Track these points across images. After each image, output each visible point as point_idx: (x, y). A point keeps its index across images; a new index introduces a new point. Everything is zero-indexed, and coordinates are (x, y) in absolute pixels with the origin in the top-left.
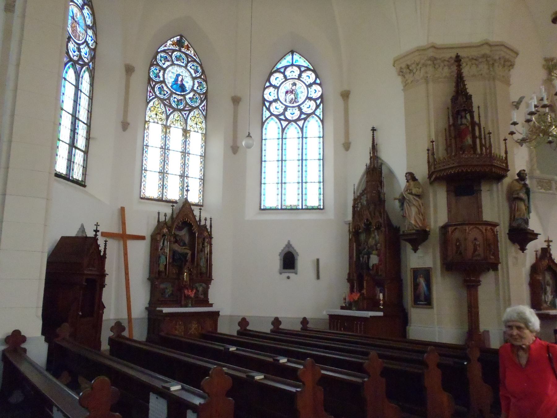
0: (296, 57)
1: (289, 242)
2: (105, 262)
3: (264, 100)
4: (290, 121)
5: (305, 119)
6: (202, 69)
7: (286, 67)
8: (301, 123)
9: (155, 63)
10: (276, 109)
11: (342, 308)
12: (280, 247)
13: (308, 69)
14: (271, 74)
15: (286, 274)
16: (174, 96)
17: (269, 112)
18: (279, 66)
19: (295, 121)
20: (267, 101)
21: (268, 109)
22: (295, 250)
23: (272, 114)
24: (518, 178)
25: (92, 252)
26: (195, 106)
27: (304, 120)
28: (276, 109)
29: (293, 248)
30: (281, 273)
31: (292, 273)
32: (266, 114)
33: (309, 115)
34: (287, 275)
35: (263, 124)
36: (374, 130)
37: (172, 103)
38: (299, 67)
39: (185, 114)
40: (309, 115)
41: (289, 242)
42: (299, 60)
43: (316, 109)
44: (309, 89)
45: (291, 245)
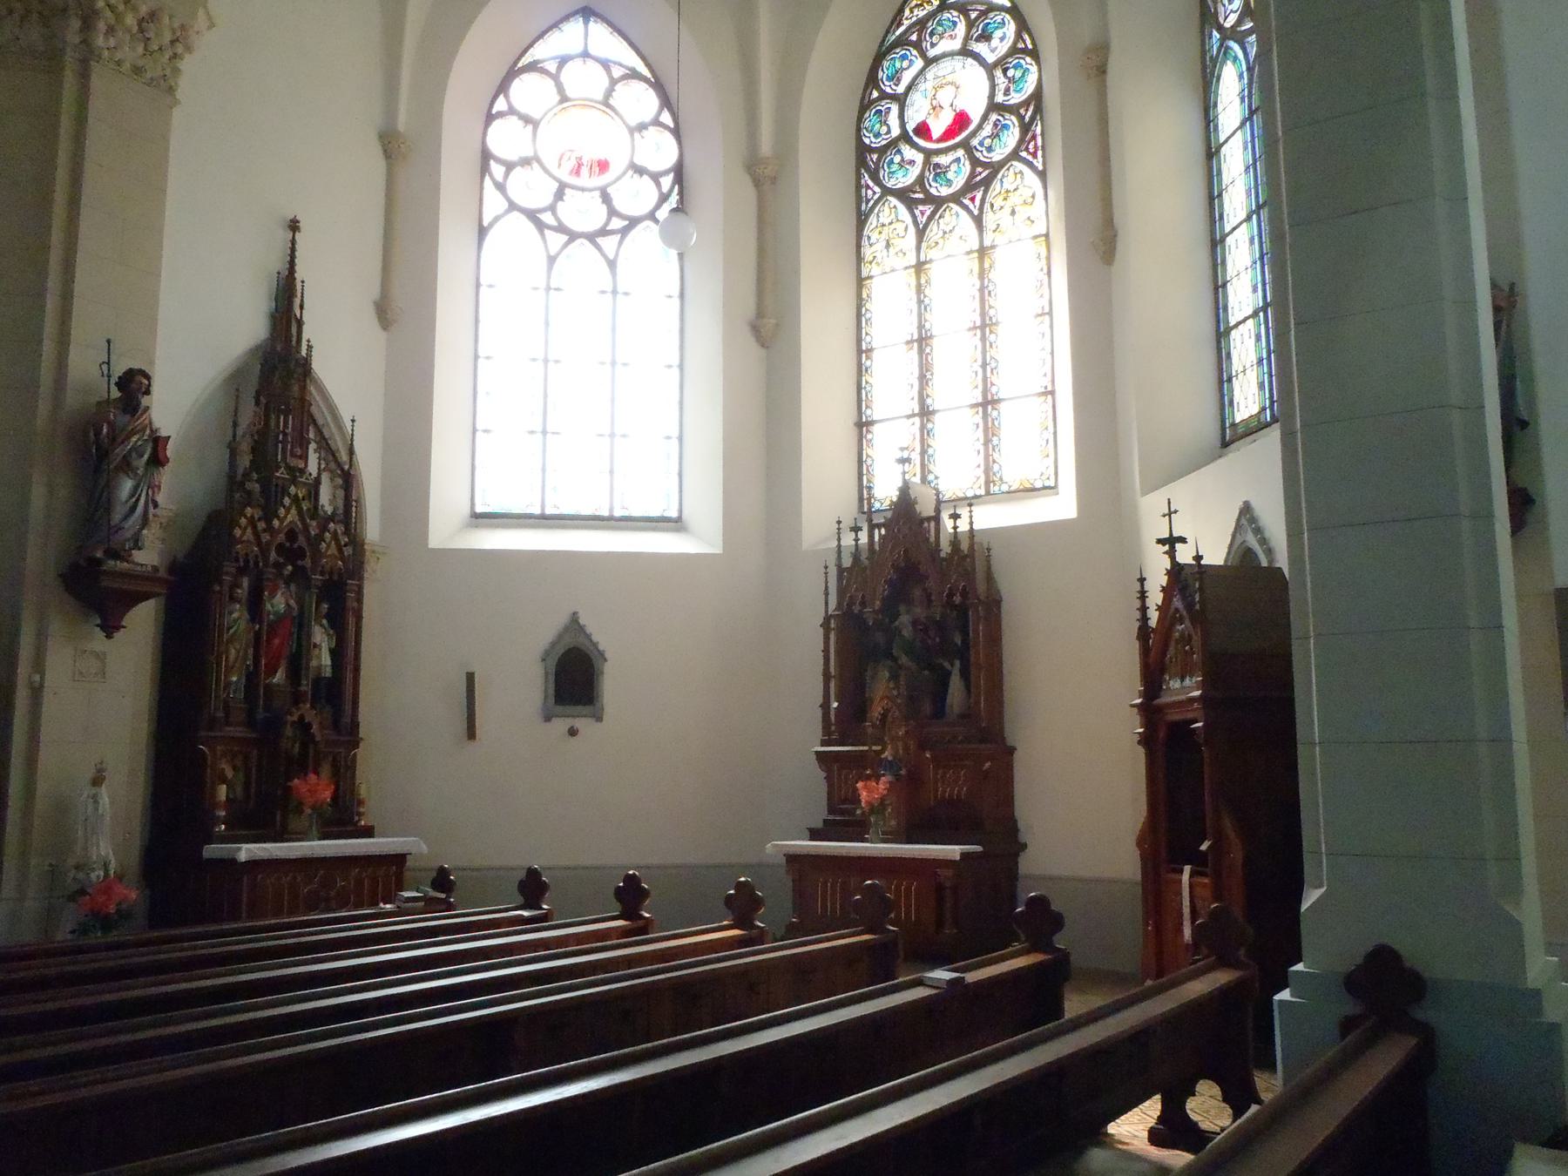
0: (598, 30)
1: (574, 618)
2: (1146, 763)
3: (486, 156)
4: (573, 236)
5: (624, 232)
6: (892, 49)
7: (563, 61)
8: (609, 243)
9: (973, 15)
10: (531, 188)
11: (815, 835)
12: (544, 632)
13: (634, 75)
14: (512, 73)
15: (566, 719)
16: (975, 142)
17: (910, 213)
18: (538, 52)
19: (592, 237)
20: (499, 161)
21: (501, 187)
22: (595, 645)
23: (513, 206)
24: (120, 394)
25: (884, 716)
26: (882, 178)
27: (622, 234)
28: (531, 188)
29: (588, 637)
30: (548, 719)
31: (585, 716)
32: (493, 203)
33: (633, 222)
34: (569, 722)
35: (482, 232)
36: (109, 342)
37: (989, 160)
38: (606, 65)
39: (973, 203)
40: (633, 222)
41: (574, 618)
42: (603, 40)
43: (658, 206)
44: (637, 135)
45: (582, 629)
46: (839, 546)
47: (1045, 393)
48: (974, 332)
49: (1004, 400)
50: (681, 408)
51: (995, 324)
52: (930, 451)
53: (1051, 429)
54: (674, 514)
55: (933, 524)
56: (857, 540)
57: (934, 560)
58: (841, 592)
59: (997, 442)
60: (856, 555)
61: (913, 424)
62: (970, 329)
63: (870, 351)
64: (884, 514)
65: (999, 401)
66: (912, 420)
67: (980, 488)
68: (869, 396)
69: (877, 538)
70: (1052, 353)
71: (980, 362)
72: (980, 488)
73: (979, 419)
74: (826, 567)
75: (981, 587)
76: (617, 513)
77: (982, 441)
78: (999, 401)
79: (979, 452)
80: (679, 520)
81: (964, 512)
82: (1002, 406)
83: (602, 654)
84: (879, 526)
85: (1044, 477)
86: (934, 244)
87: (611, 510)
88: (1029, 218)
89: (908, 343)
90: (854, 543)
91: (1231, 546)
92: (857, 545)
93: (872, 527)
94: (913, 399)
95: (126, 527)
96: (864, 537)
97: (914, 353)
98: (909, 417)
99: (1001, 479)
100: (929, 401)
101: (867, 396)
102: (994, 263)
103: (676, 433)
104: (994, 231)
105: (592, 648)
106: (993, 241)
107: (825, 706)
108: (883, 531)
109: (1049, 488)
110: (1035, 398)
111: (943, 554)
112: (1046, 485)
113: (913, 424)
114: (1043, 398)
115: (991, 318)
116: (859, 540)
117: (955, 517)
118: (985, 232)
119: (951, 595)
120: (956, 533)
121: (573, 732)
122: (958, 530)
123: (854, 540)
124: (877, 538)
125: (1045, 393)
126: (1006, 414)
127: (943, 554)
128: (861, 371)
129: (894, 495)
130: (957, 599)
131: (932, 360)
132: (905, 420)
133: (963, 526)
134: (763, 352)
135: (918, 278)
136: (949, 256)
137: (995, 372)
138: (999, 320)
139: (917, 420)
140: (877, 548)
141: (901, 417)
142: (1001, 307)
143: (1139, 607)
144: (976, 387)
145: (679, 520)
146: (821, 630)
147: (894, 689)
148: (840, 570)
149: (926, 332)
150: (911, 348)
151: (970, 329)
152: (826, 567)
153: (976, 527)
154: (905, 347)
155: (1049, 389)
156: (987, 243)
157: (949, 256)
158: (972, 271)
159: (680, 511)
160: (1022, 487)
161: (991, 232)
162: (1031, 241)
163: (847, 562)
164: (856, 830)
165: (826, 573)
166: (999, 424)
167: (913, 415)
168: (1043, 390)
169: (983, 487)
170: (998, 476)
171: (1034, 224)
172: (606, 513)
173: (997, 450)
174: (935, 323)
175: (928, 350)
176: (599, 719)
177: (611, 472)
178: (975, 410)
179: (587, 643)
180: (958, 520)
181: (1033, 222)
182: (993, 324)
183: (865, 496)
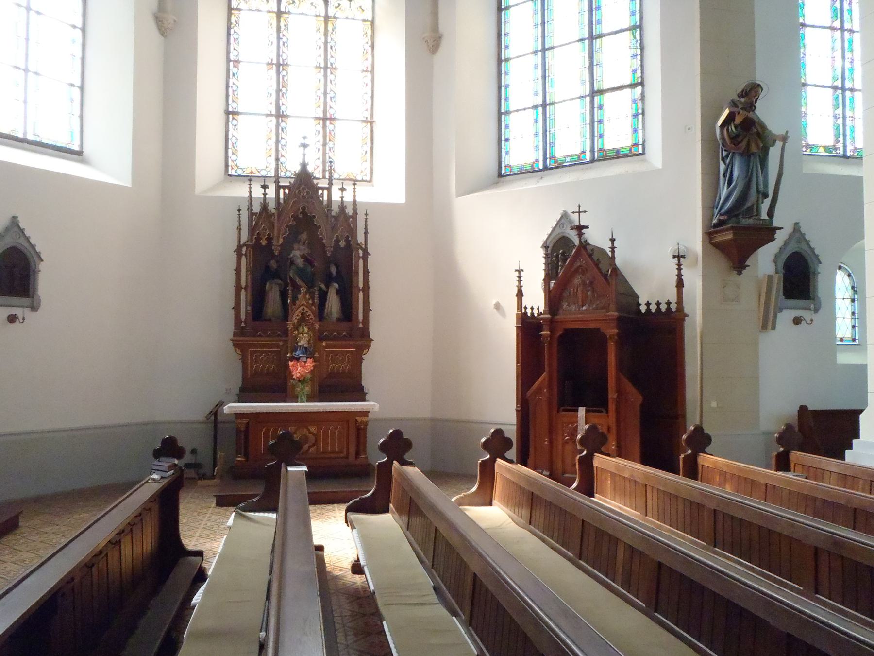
29: (27, 239)
46: (251, 197)
47: (366, 122)
48: (320, 70)
49: (338, 119)
50: (27, 55)
51: (334, 69)
52: (283, 142)
53: (369, 144)
54: (76, 148)
55: (326, 192)
56: (265, 194)
57: (327, 216)
58: (252, 230)
59: (333, 146)
60: (264, 206)
61: (271, 121)
62: (316, 67)
63: (237, 62)
64: (289, 180)
65: (287, 116)
66: (270, 118)
67: (319, 173)
68: (235, 94)
69: (282, 196)
70: (372, 97)
71: (322, 90)
72: (319, 173)
73: (320, 128)
74: (239, 210)
75: (361, 239)
76: (30, 137)
77: (321, 143)
78: (287, 116)
79: (319, 150)
80: (79, 153)
81: (349, 187)
82: (289, 120)
83: (38, 255)
84: (284, 187)
85: (268, 169)
86: (292, 2)
87: (25, 133)
88: (361, 7)
89: (268, 64)
90: (263, 196)
91: (550, 235)
92: (265, 198)
93: (278, 187)
94: (271, 104)
95: (859, 144)
96: (271, 193)
97: (273, 72)
98: (267, 115)
99: (285, 168)
100: (283, 108)
101: (233, 93)
102: (335, 28)
103: (78, 83)
104: (336, 8)
105: (31, 250)
106: (335, 13)
107: (237, 308)
108: (287, 191)
109: (366, 181)
110: (360, 123)
111: (333, 213)
112: (364, 179)
113: (271, 121)
114: (364, 124)
115: (331, 64)
116: (266, 194)
117: (342, 189)
118: (329, 6)
119: (337, 241)
120: (342, 201)
121: (12, 319)
122: (267, 196)
123: (263, 194)
124: (282, 196)
125: (366, 122)
126: (339, 129)
127: (333, 213)
128: (229, 75)
129: (297, 168)
130: (264, 242)
131: (287, 80)
132: (264, 117)
133: (348, 197)
134: (162, 38)
135: (278, 22)
136: (302, 14)
137: (333, 100)
138: (337, 67)
139: (274, 119)
140: (282, 201)
141: (262, 115)
142: (339, 58)
143: (682, 270)
144: (319, 106)
145: (79, 153)
146: (235, 255)
147: (309, 299)
148: (251, 214)
149: (283, 60)
150: (271, 69)
151: (316, 67)
152: (239, 210)
153: (358, 199)
154: (265, 67)
155: (369, 119)
156: (331, 14)
157: (302, 14)
158: (319, 29)
159: (81, 146)
160: (348, 178)
161: (334, 7)
162: (361, 22)
163: (257, 209)
164: (282, 391)
165: (366, 219)
166: (334, 134)
167: (271, 115)
168: (365, 119)
169: (321, 173)
170: (284, 165)
171: (364, 12)
172: (21, 135)
173: (332, 151)
174: (290, 55)
175: (284, 73)
176: (34, 308)
177: (25, 102)
178: (318, 121)
179: (26, 245)
180: (344, 192)
181: (363, 10)
182: (332, 68)
183: (328, 168)
